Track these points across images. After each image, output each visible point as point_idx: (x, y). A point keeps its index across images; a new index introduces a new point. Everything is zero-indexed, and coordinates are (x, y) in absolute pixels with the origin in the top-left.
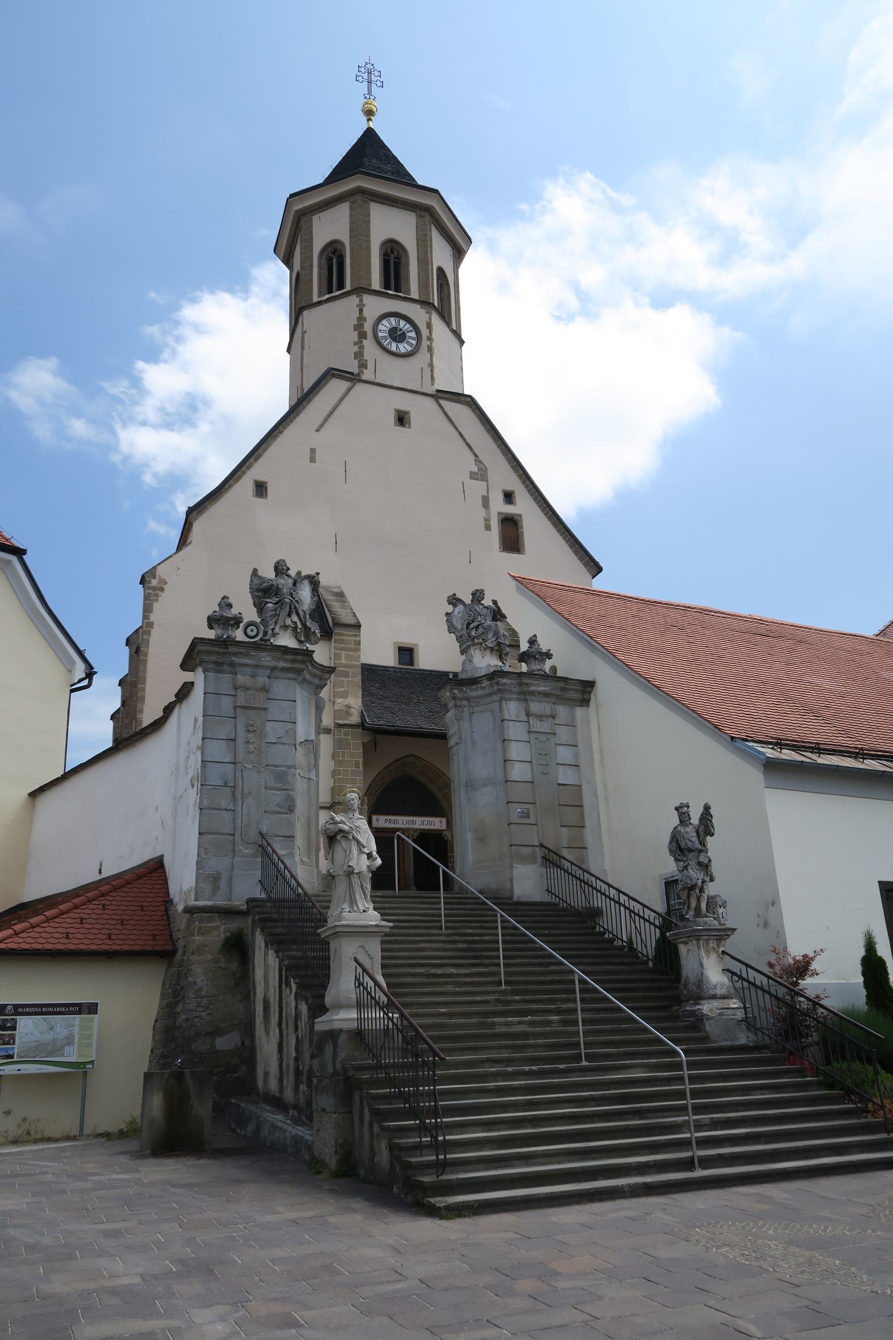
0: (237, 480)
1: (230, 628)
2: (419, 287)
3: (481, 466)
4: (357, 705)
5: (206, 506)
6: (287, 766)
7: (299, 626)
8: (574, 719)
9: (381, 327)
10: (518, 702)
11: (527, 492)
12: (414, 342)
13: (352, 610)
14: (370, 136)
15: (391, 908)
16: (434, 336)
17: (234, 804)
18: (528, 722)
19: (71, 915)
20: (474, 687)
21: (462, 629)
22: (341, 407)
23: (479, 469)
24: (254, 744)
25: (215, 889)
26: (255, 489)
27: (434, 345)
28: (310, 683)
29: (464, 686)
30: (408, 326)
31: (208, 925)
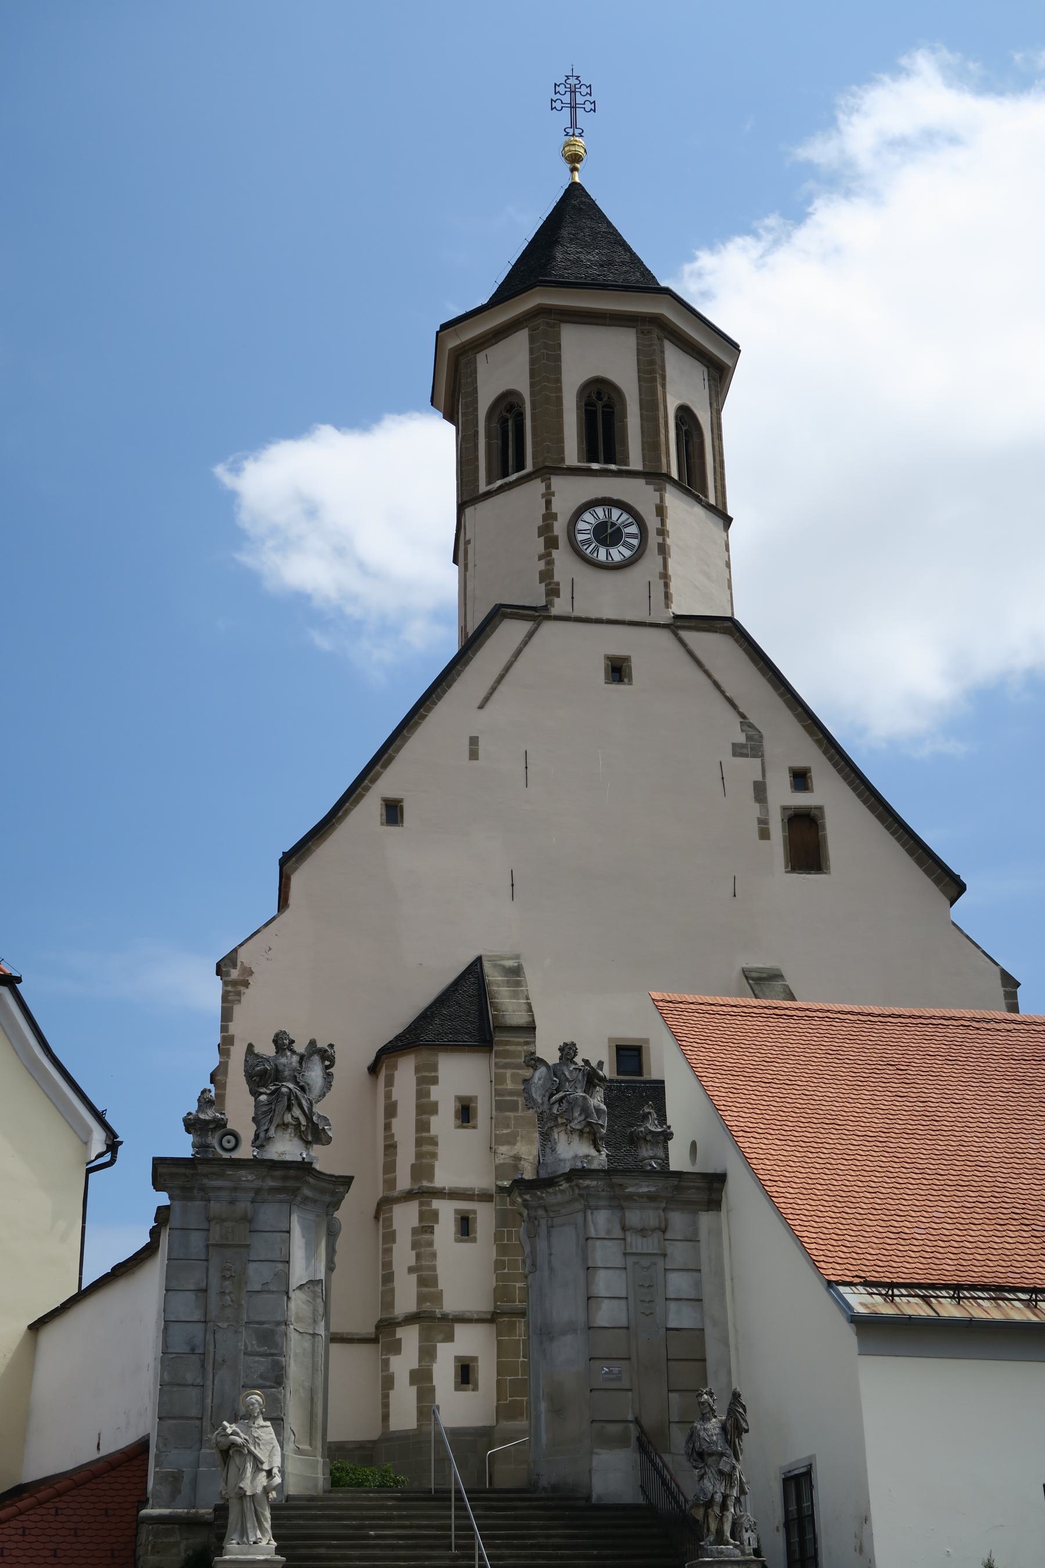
0: (357, 801)
1: (210, 1133)
2: (643, 449)
3: (752, 732)
4: (530, 1154)
5: (309, 848)
6: (275, 1322)
7: (303, 1121)
8: (696, 1231)
9: (581, 525)
10: (610, 1211)
11: (832, 767)
12: (635, 542)
13: (528, 999)
14: (575, 191)
15: (400, 1517)
16: (669, 525)
17: (203, 1377)
18: (624, 1239)
19: (13, 1524)
20: (551, 1190)
21: (542, 1104)
22: (517, 665)
23: (749, 738)
24: (232, 1295)
25: (175, 1492)
26: (384, 814)
27: (669, 541)
28: (315, 1201)
29: (538, 1189)
30: (625, 516)
31: (165, 1540)
